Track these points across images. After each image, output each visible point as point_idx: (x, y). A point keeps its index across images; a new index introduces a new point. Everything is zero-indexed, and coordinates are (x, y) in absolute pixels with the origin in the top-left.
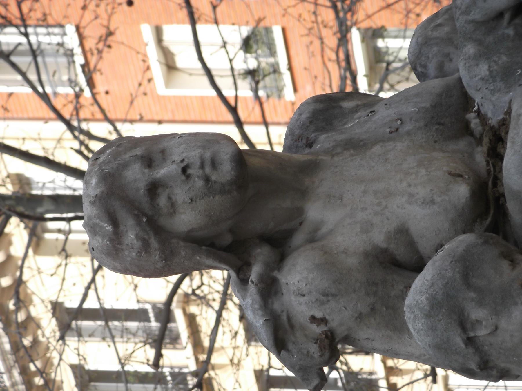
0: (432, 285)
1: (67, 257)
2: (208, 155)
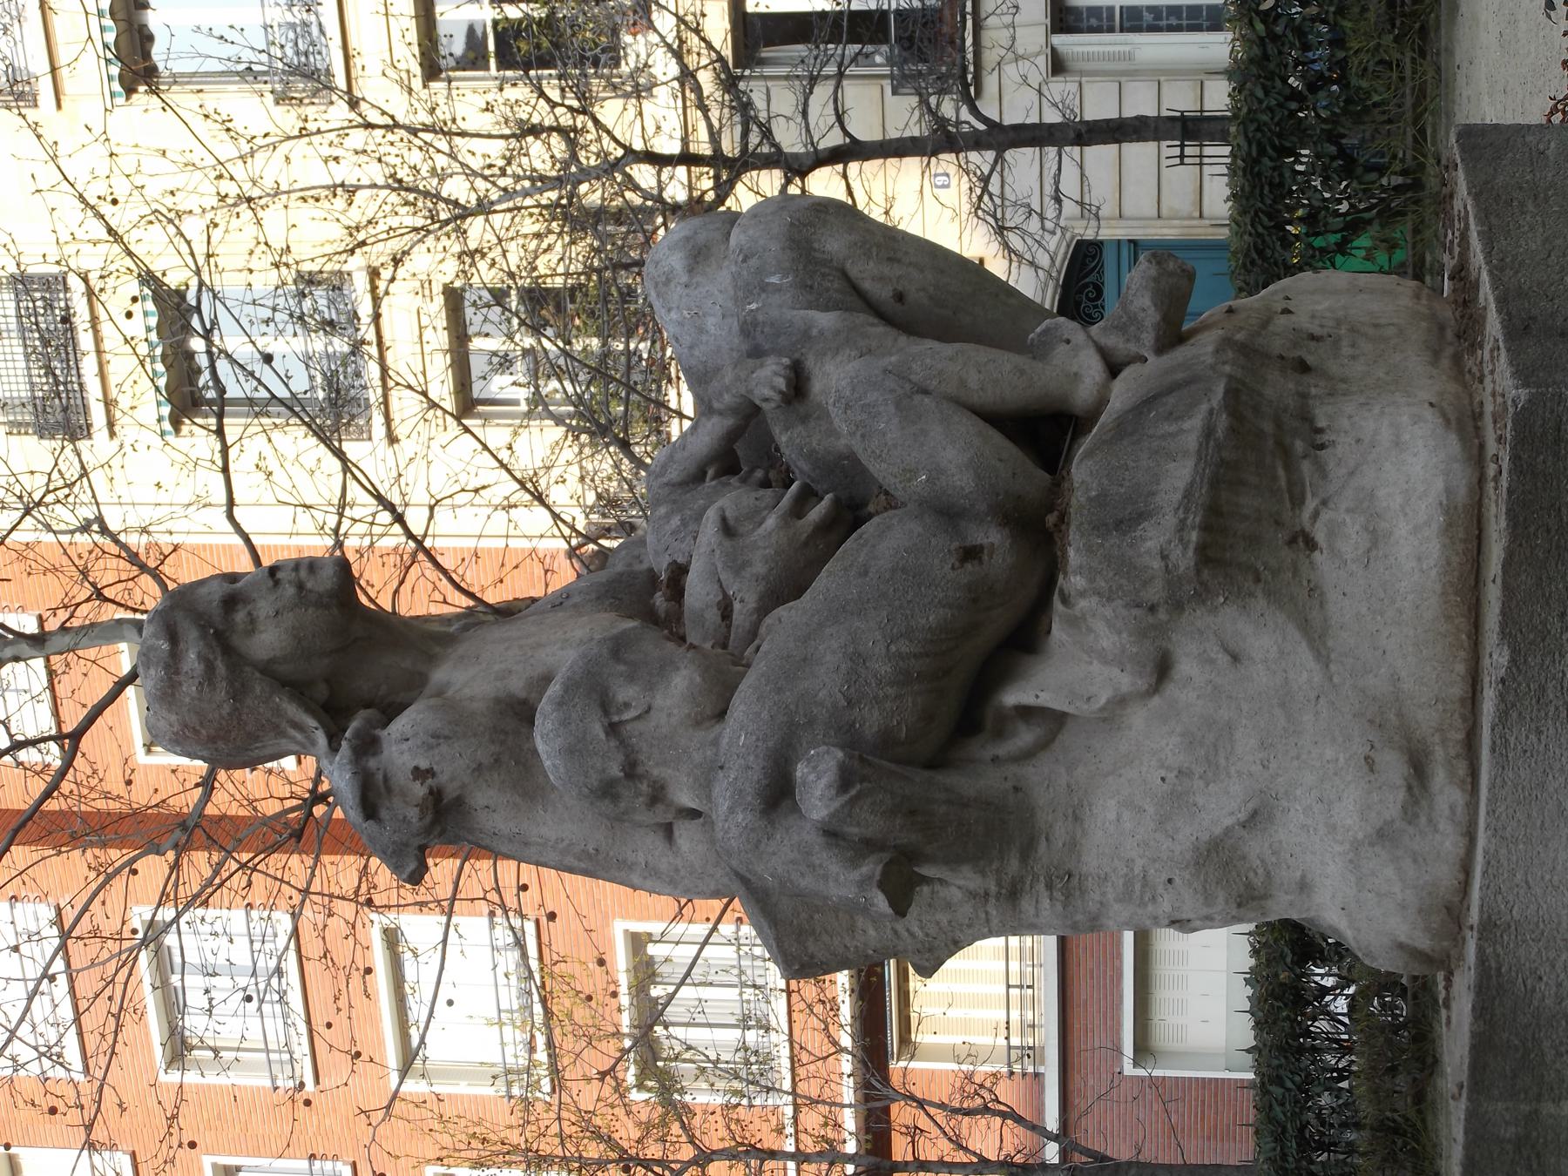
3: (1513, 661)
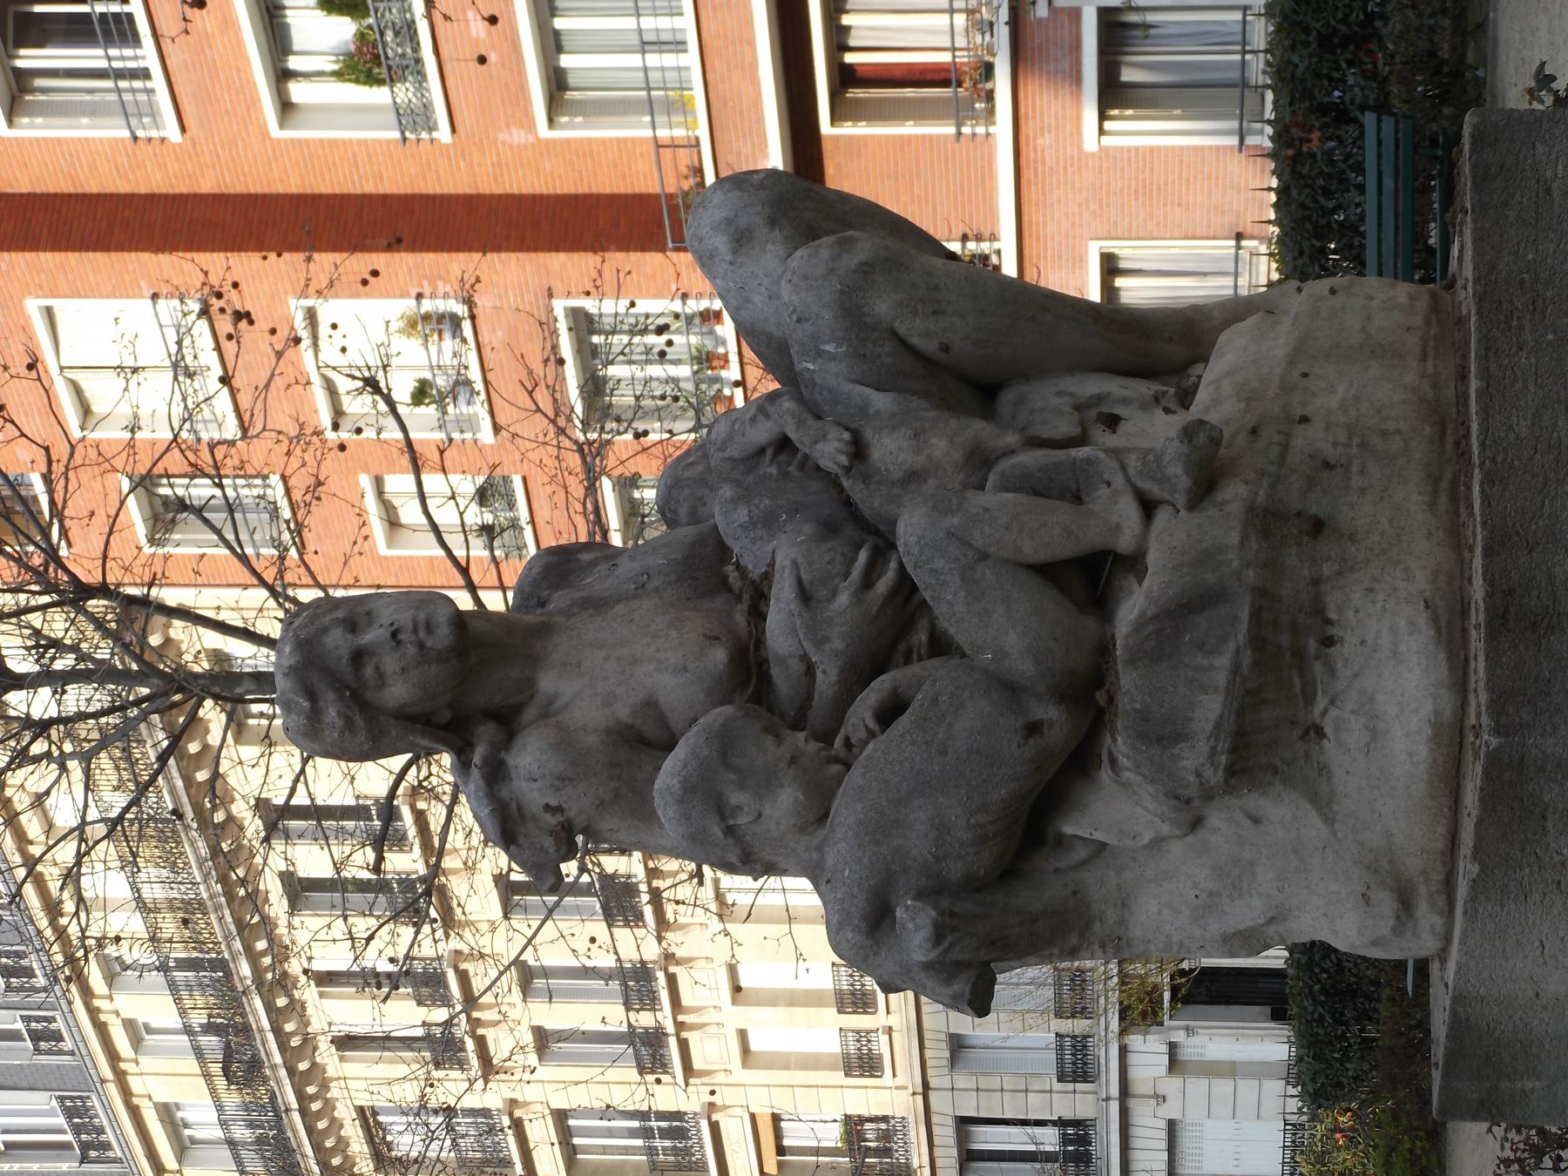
0: (685, 766)
1: (270, 746)
2: (422, 617)
3: (1482, 870)
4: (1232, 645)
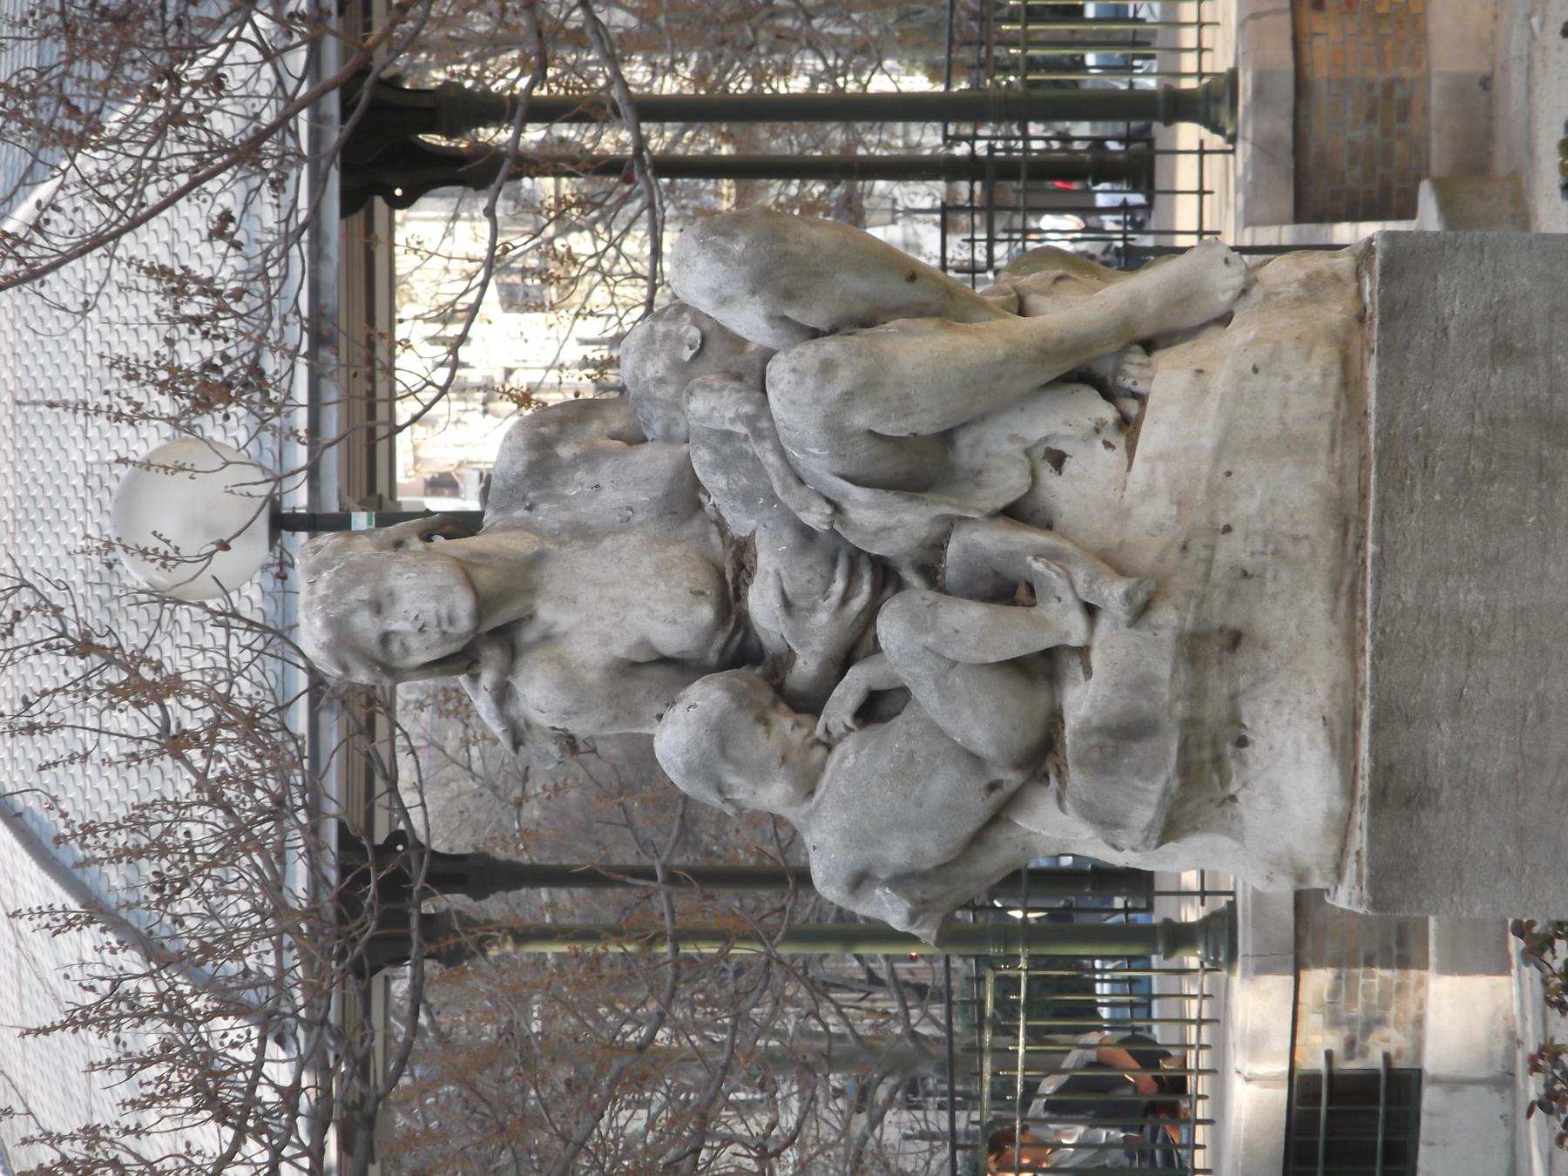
2: (444, 612)
4: (1163, 777)
